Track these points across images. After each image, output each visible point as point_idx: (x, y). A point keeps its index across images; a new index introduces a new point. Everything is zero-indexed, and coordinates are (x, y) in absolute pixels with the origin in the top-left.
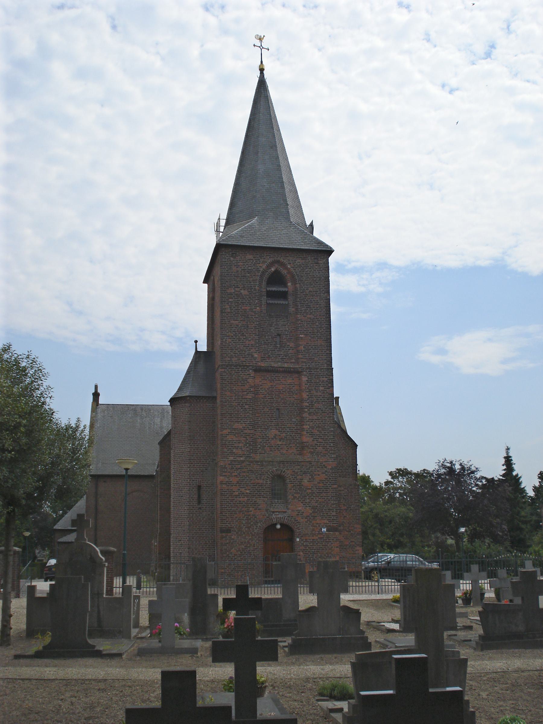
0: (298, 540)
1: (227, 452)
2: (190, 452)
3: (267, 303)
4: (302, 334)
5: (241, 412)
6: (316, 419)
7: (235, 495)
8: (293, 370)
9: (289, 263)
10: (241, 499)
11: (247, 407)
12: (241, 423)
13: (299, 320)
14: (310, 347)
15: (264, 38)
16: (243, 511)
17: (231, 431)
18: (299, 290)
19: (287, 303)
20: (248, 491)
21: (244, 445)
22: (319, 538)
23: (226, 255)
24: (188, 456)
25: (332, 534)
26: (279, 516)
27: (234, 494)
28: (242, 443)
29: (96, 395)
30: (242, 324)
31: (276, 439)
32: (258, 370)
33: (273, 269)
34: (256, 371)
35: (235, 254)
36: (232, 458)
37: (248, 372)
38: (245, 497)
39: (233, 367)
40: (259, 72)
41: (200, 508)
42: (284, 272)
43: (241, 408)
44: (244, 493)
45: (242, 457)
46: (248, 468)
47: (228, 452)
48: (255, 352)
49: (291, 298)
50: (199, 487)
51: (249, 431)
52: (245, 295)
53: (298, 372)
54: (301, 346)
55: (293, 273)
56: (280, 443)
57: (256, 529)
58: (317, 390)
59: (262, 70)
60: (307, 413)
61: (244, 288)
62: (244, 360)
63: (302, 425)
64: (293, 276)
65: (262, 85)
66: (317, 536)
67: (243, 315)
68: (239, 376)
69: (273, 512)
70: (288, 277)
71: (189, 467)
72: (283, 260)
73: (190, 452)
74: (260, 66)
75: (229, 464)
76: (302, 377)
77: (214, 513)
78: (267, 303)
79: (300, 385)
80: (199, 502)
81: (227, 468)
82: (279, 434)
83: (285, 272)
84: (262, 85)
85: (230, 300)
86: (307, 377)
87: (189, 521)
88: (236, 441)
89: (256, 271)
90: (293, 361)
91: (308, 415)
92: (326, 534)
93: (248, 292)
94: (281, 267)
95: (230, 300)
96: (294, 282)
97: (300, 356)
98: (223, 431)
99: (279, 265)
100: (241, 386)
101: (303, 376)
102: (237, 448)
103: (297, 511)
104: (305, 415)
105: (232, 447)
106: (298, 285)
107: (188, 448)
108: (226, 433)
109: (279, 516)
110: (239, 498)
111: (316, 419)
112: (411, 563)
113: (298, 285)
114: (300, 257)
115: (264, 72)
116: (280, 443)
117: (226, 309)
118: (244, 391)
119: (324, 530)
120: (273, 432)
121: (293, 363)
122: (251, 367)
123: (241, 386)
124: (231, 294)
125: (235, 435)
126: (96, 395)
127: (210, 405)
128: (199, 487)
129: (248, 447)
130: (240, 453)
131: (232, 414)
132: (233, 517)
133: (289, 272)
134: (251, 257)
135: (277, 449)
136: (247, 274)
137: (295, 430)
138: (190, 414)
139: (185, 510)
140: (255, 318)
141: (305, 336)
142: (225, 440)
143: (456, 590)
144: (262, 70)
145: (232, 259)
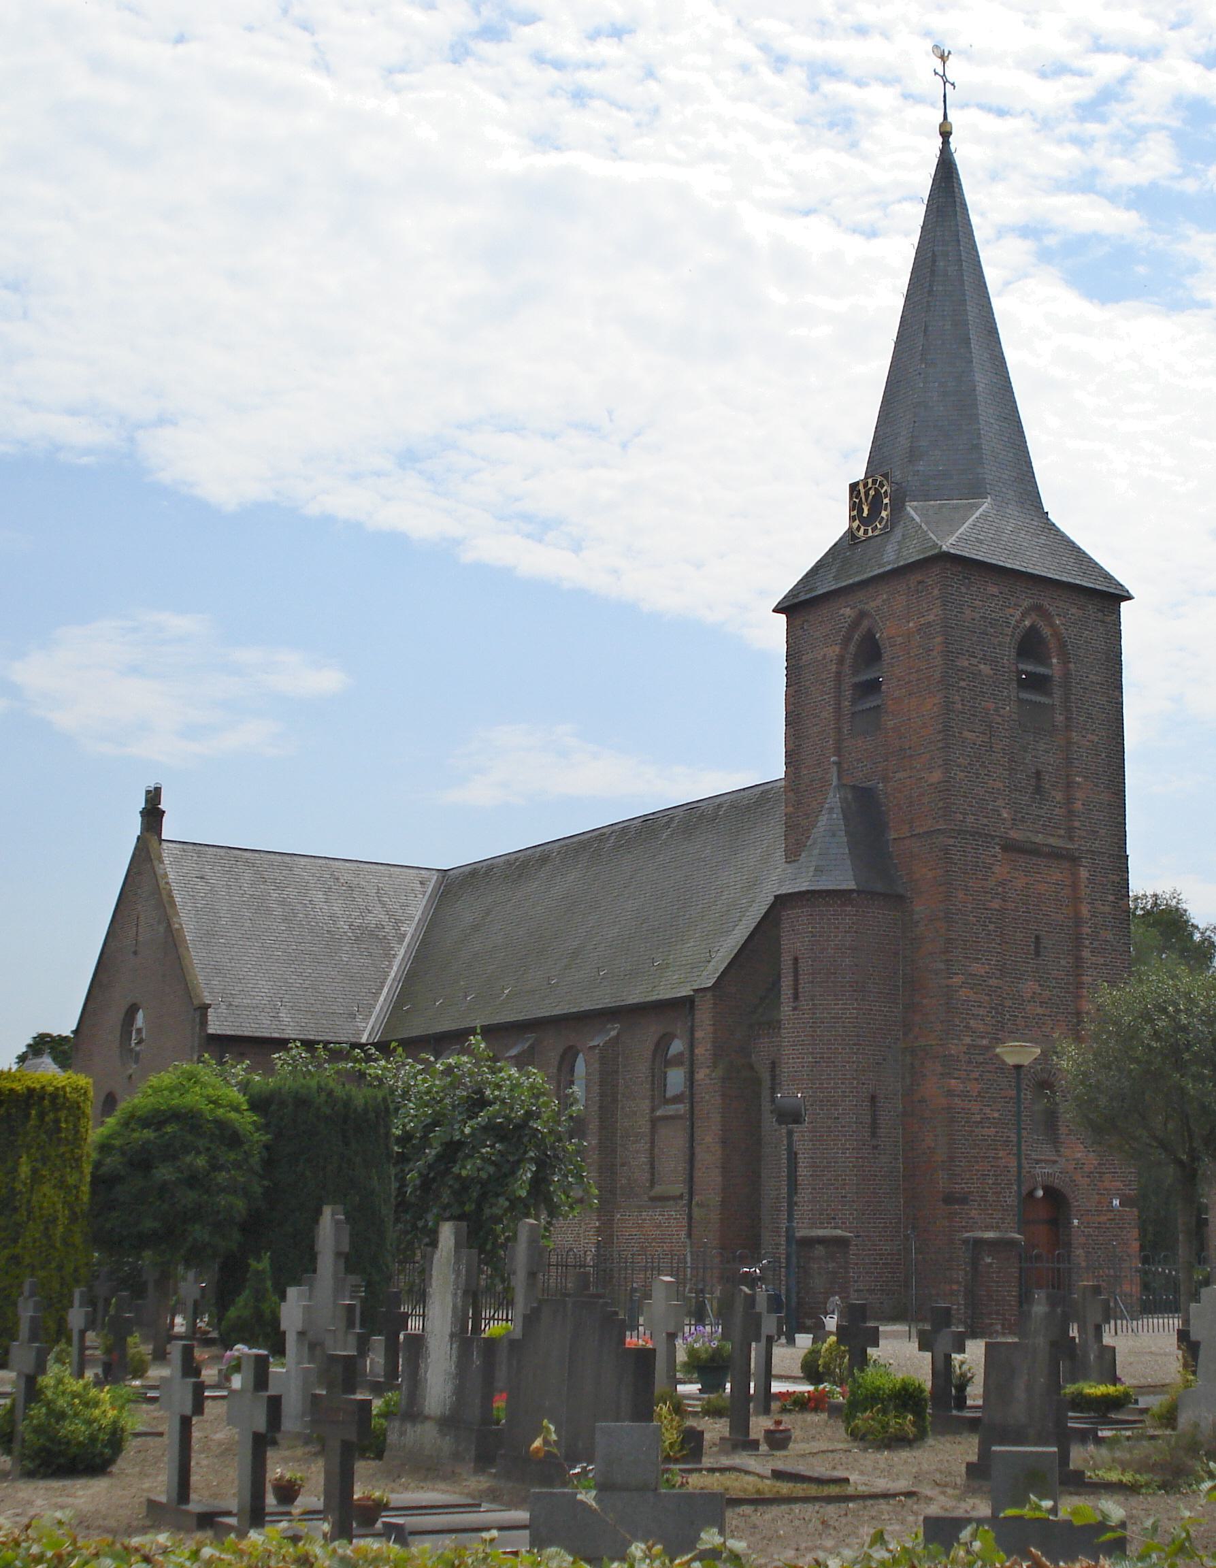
0: (1076, 1222)
1: (960, 1026)
2: (857, 1018)
3: (1018, 698)
4: (1079, 776)
5: (982, 938)
6: (1102, 965)
7: (974, 1122)
8: (1065, 853)
9: (1057, 615)
10: (986, 1131)
11: (992, 927)
12: (983, 964)
13: (1075, 743)
14: (1092, 805)
15: (950, 56)
16: (988, 1157)
17: (966, 979)
18: (1073, 677)
19: (1051, 702)
20: (996, 1115)
21: (988, 1012)
22: (1109, 1220)
23: (953, 578)
24: (855, 1027)
25: (1129, 1212)
26: (1046, 1171)
27: (973, 1120)
28: (985, 1007)
29: (152, 814)
30: (982, 741)
31: (1034, 1002)
32: (1010, 847)
33: (1027, 623)
34: (1005, 849)
35: (969, 579)
36: (968, 1040)
37: (993, 850)
38: (990, 1127)
39: (968, 837)
40: (941, 140)
41: (875, 1147)
42: (1046, 631)
43: (983, 930)
44: (989, 1118)
45: (983, 1037)
46: (995, 1064)
47: (962, 1025)
48: (1004, 807)
49: (1058, 693)
50: (873, 1098)
51: (996, 981)
52: (986, 676)
53: (1073, 859)
54: (1077, 802)
55: (1064, 637)
56: (1040, 1011)
57: (1010, 1197)
58: (1104, 901)
59: (946, 134)
60: (1089, 950)
61: (984, 660)
62: (985, 821)
63: (1078, 975)
64: (1062, 645)
65: (946, 172)
66: (1106, 1215)
67: (984, 722)
68: (978, 858)
69: (1038, 1161)
70: (1053, 644)
71: (855, 1053)
72: (1048, 606)
73: (857, 1018)
74: (941, 126)
75: (964, 1053)
76: (1079, 870)
77: (898, 1159)
78: (1018, 698)
79: (1075, 886)
80: (874, 1135)
81: (961, 1061)
82: (1040, 991)
83: (1049, 633)
84: (946, 172)
85: (962, 684)
86: (1089, 871)
87: (856, 1175)
88: (975, 1002)
89: (1005, 624)
90: (1062, 832)
91: (1089, 954)
92: (1119, 1211)
93: (992, 669)
94: (1042, 621)
95: (962, 684)
96: (1065, 659)
97: (1077, 824)
98: (952, 978)
99: (1037, 615)
100: (982, 879)
101: (1082, 868)
102: (975, 1016)
103: (1074, 1160)
104: (1086, 954)
105: (967, 1014)
106: (1072, 666)
107: (853, 1009)
108: (958, 982)
109: (1046, 1171)
110: (983, 1127)
111: (1102, 965)
112: (689, 1269)
113: (1072, 666)
114: (1075, 604)
115: (951, 139)
116: (1040, 1011)
117: (955, 703)
118: (987, 892)
119: (1116, 1202)
120: (1029, 987)
121: (1059, 836)
122: (997, 840)
123: (982, 879)
124: (963, 670)
125: (972, 989)
126: (152, 814)
127: (889, 915)
128: (873, 1098)
129: (993, 1017)
130: (982, 1030)
131: (966, 941)
132: (972, 1171)
133: (1056, 634)
134: (994, 590)
135: (1037, 1023)
136: (989, 629)
137: (1065, 984)
138: (856, 932)
139: (848, 1149)
140: (1003, 731)
141: (1085, 781)
142: (956, 999)
143: (628, 1333)
144: (946, 134)
145: (963, 590)
